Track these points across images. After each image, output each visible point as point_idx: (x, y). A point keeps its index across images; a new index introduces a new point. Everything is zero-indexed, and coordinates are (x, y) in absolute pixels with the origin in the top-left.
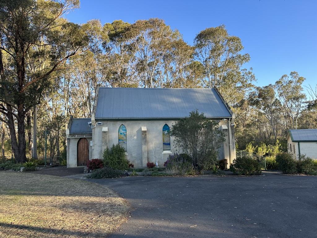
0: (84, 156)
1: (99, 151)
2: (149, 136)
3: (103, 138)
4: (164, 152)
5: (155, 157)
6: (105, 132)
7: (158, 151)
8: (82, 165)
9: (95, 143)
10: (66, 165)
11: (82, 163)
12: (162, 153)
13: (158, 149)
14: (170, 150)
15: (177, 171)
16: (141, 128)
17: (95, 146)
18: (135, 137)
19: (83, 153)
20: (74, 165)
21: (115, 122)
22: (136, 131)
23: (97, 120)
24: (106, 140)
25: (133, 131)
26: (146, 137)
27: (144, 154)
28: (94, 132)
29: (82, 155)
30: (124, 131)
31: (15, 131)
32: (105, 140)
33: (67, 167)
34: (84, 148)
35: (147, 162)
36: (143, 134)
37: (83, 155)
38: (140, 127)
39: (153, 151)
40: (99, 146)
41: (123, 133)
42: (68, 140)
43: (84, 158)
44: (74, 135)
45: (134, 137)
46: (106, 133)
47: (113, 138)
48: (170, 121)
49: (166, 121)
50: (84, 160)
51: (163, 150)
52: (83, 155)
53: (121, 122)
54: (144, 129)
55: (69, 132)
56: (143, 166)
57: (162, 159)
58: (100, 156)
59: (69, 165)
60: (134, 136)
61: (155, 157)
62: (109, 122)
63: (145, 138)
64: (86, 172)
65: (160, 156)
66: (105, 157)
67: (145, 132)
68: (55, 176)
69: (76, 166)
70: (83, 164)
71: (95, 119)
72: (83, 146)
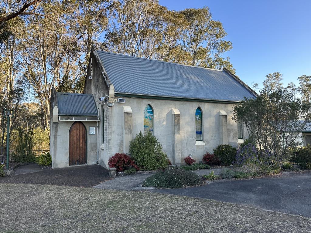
0: (78, 150)
1: (119, 141)
2: (182, 122)
3: (125, 122)
4: (196, 143)
5: (187, 149)
6: (128, 113)
7: (191, 141)
8: (75, 164)
9: (113, 130)
10: (51, 164)
11: (76, 160)
12: (195, 144)
13: (190, 139)
14: (202, 140)
15: (259, 169)
16: (172, 110)
17: (113, 134)
18: (165, 123)
19: (77, 144)
20: (65, 163)
21: (140, 100)
22: (166, 114)
23: (116, 95)
24: (130, 125)
25: (163, 112)
26: (179, 123)
27: (177, 146)
28: (112, 114)
29: (76, 147)
30: (150, 114)
31: (87, 71)
32: (129, 125)
33: (53, 168)
34: (78, 137)
35: (180, 156)
36: (175, 118)
37: (77, 148)
38: (171, 109)
39: (185, 142)
40: (118, 135)
41: (148, 116)
42: (55, 126)
43: (78, 152)
44: (71, 117)
45: (163, 123)
46: (130, 115)
47: (137, 122)
48: (203, 104)
49: (199, 103)
50: (78, 156)
51: (196, 141)
52: (77, 148)
53: (147, 100)
54: (176, 111)
55: (58, 112)
56: (176, 162)
57: (195, 152)
58: (120, 149)
59: (57, 165)
60: (164, 121)
61: (187, 149)
62: (132, 100)
63: (178, 124)
64: (113, 175)
65: (192, 148)
66: (132, 150)
67: (178, 115)
68: (81, 188)
69: (68, 166)
70: (77, 161)
71: (115, 93)
72: (77, 135)
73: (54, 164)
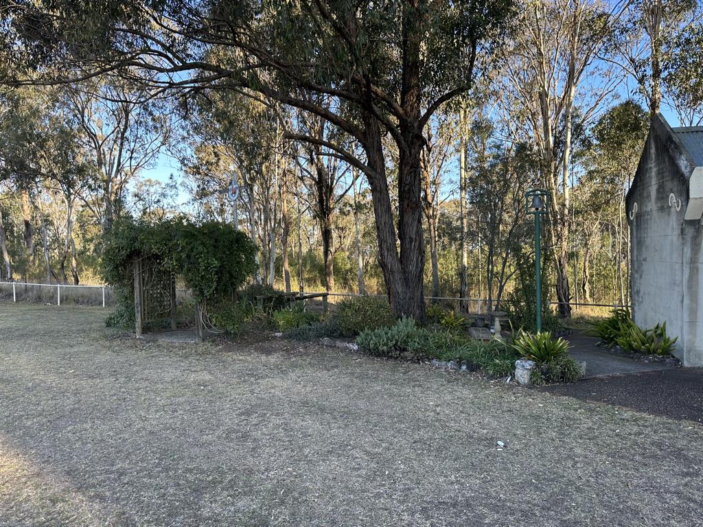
73: (689, 351)
